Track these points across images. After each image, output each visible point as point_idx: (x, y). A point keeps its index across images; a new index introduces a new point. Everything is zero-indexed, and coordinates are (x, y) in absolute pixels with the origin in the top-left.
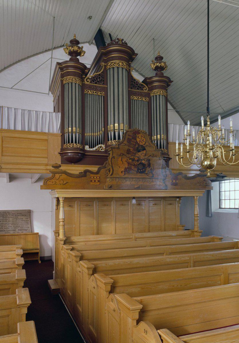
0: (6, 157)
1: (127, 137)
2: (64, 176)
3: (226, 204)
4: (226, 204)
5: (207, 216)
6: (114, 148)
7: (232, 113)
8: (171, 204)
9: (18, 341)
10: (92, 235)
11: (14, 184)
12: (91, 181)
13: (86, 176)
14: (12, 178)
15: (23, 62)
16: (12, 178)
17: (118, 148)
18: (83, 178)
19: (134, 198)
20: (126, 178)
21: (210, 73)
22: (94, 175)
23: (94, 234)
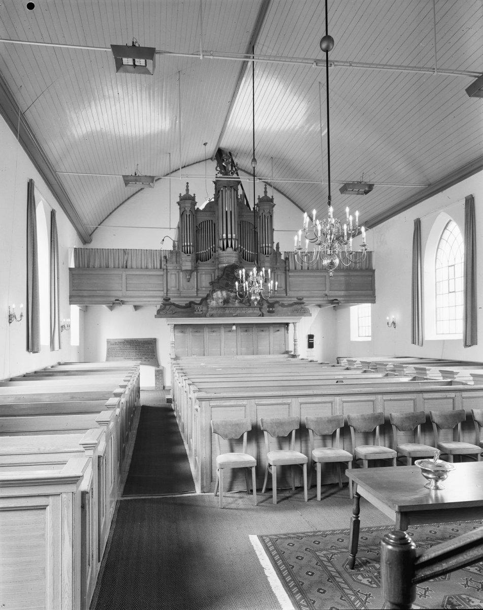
0: (129, 292)
1: (226, 272)
2: (173, 307)
3: (354, 337)
4: (354, 337)
5: (414, 342)
6: (214, 283)
7: (463, 176)
8: (278, 331)
9: (240, 61)
10: (251, 354)
11: (139, 312)
12: (195, 311)
13: (190, 307)
14: (136, 308)
15: (125, 203)
16: (136, 308)
17: (218, 282)
18: (188, 309)
19: (234, 324)
20: (225, 307)
21: (331, 191)
22: (197, 306)
23: (271, 352)
